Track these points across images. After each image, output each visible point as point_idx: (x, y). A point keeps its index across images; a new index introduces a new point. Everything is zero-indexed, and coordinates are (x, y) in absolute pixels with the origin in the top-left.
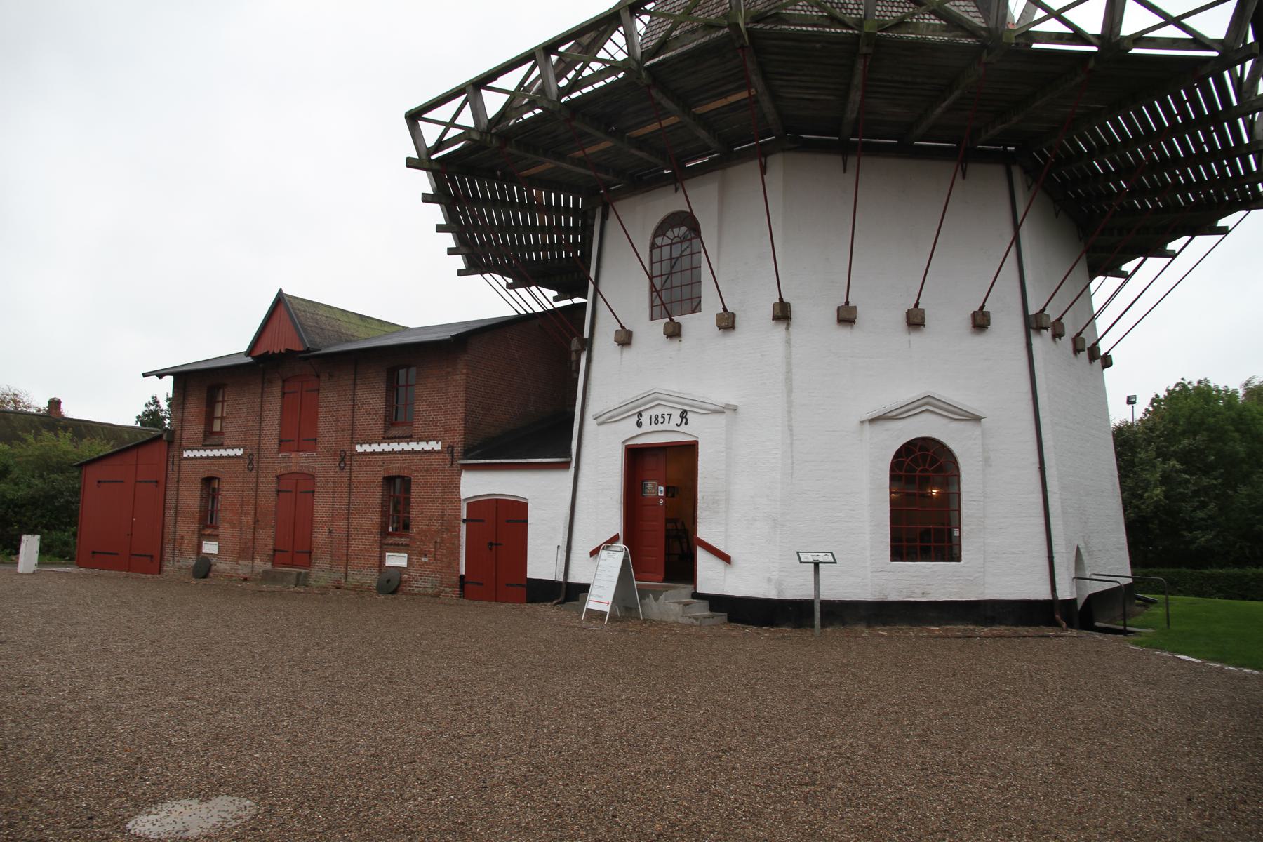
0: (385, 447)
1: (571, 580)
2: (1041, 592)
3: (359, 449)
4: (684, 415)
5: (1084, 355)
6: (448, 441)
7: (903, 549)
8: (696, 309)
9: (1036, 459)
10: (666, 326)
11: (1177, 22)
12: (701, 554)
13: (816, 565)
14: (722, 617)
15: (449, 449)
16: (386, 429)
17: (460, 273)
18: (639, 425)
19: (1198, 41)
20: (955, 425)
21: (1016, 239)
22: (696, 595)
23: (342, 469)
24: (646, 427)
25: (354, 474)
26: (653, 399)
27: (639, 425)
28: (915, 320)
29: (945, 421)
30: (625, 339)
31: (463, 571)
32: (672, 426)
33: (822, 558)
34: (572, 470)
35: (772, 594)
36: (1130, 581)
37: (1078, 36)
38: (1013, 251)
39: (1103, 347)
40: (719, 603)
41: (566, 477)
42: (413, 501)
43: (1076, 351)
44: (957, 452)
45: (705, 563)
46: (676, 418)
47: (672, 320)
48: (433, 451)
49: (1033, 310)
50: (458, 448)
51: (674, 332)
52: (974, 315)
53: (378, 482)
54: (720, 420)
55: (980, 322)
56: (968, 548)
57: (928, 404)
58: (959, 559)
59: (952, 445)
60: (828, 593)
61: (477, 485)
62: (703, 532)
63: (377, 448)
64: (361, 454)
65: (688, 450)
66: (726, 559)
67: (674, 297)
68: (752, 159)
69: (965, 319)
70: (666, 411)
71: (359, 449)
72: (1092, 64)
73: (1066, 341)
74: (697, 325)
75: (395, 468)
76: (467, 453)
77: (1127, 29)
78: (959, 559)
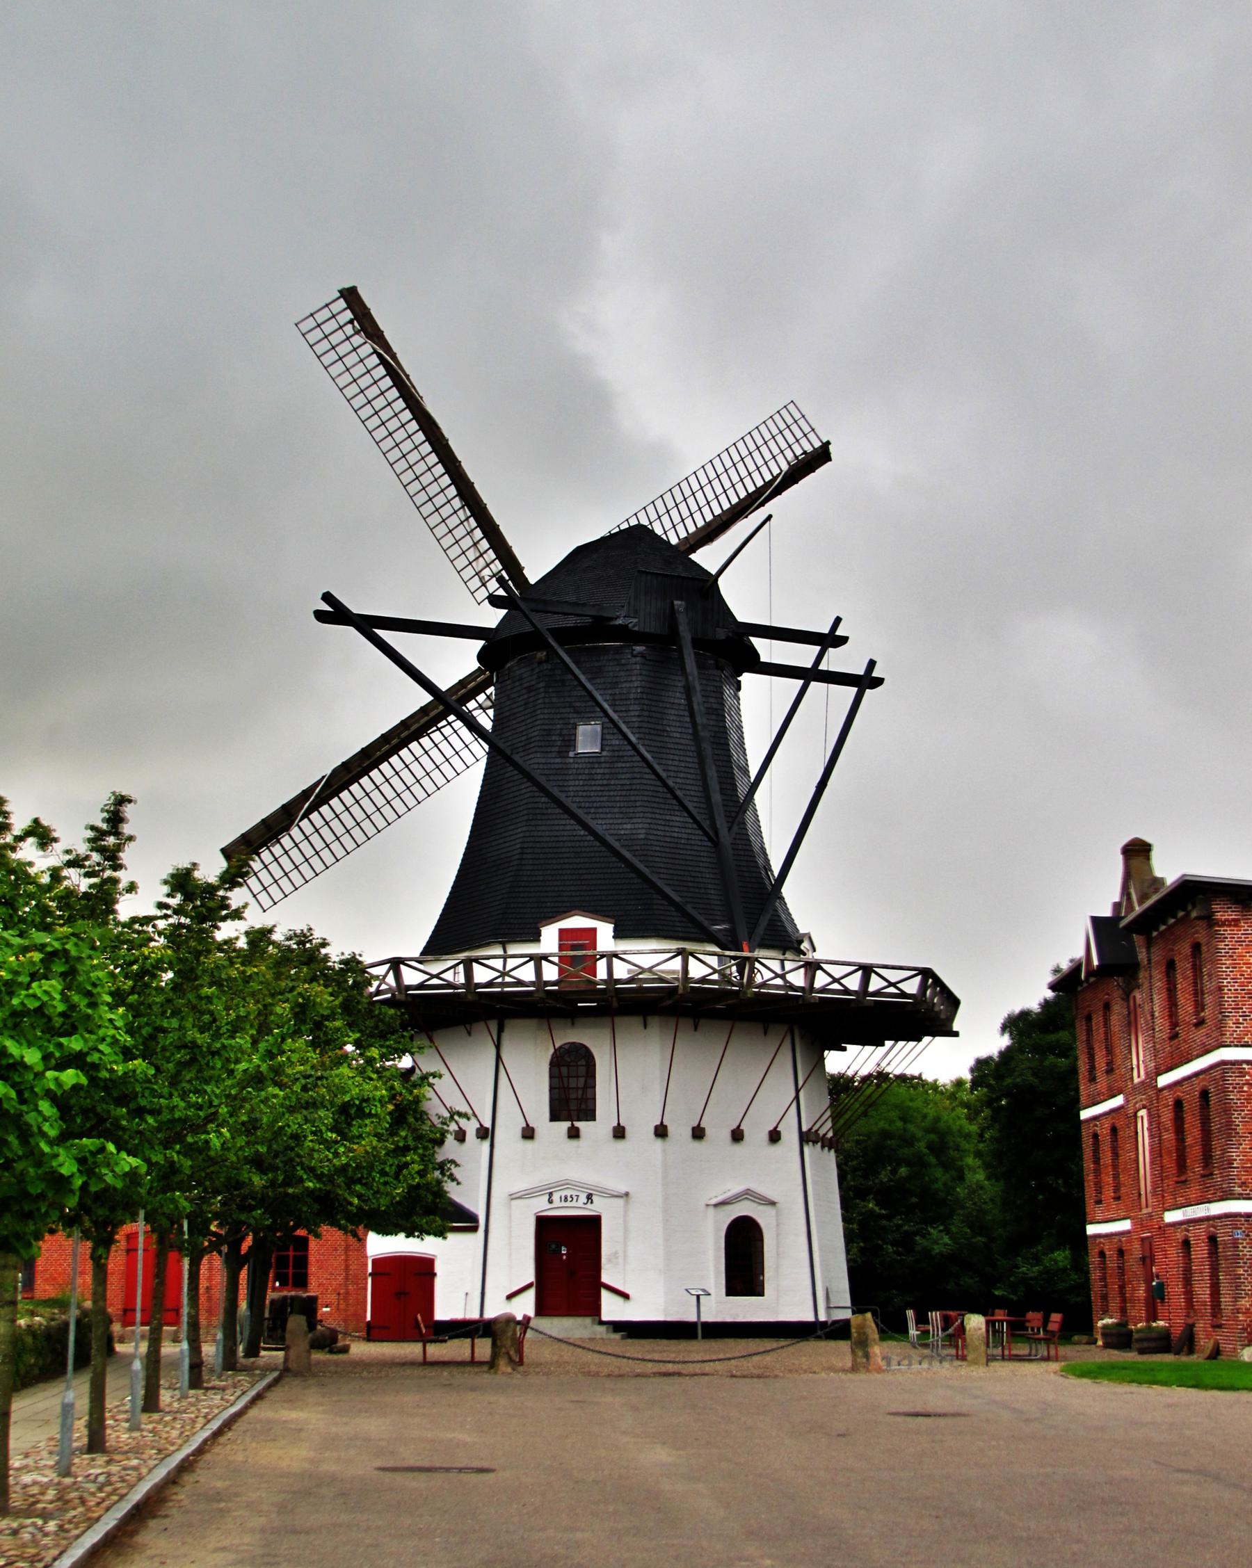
4: (589, 1197)
7: (731, 1291)
8: (590, 1115)
10: (569, 1129)
11: (894, 985)
13: (698, 1297)
14: (617, 1336)
18: (550, 1202)
19: (903, 994)
20: (761, 1207)
21: (797, 1098)
22: (601, 1323)
24: (557, 1203)
26: (566, 1184)
27: (550, 1202)
31: (369, 1318)
32: (580, 1204)
35: (661, 1318)
37: (846, 991)
38: (794, 1104)
40: (617, 1326)
46: (583, 1198)
49: (805, 1129)
51: (574, 1134)
54: (621, 1202)
55: (775, 1136)
57: (748, 1195)
58: (762, 1294)
59: (754, 1216)
60: (707, 1317)
62: (605, 1278)
66: (626, 1296)
67: (572, 1099)
69: (765, 1136)
70: (575, 1193)
72: (853, 1005)
74: (595, 1131)
77: (871, 988)
78: (762, 1294)
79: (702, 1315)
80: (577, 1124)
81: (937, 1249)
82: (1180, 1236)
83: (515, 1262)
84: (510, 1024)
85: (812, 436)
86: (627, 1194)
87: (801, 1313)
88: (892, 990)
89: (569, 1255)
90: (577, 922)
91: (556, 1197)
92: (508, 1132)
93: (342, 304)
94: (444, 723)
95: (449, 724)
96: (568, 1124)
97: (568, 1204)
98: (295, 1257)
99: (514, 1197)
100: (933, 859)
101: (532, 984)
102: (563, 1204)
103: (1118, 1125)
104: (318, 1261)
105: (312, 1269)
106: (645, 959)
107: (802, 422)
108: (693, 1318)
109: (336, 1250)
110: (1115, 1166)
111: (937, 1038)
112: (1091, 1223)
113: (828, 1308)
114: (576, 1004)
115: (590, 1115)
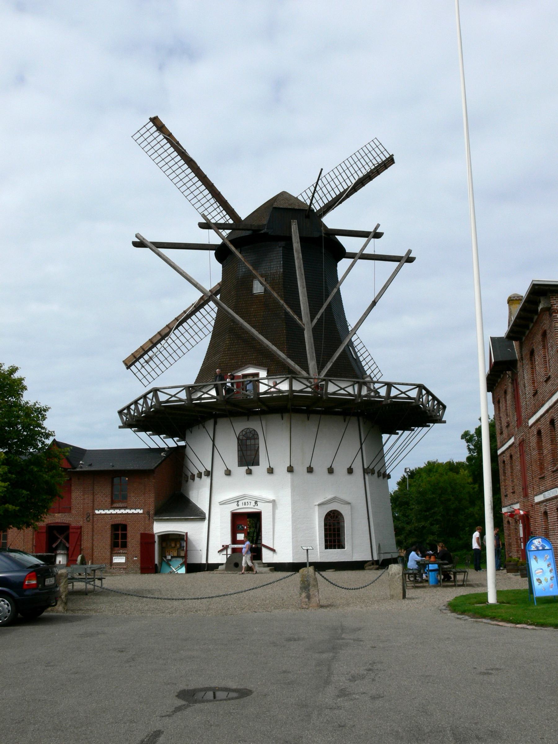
1: (210, 562)
3: (97, 512)
4: (256, 502)
6: (146, 510)
8: (257, 464)
9: (367, 515)
10: (247, 470)
11: (404, 393)
12: (264, 550)
13: (307, 550)
15: (148, 513)
17: (120, 427)
18: (238, 505)
19: (409, 398)
20: (343, 505)
21: (361, 448)
24: (241, 506)
25: (95, 523)
26: (244, 497)
27: (238, 505)
28: (331, 471)
29: (340, 504)
30: (228, 473)
32: (251, 506)
33: (309, 548)
34: (207, 521)
38: (360, 451)
39: (388, 472)
40: (269, 565)
43: (379, 476)
44: (343, 514)
48: (138, 514)
49: (366, 467)
50: (152, 512)
52: (348, 469)
53: (108, 527)
54: (271, 504)
55: (350, 471)
57: (334, 500)
59: (342, 512)
61: (160, 528)
62: (264, 542)
66: (273, 550)
67: (248, 457)
71: (97, 512)
73: (376, 474)
74: (259, 470)
75: (118, 521)
77: (392, 394)
79: (309, 559)
80: (250, 467)
81: (540, 540)
82: (542, 510)
84: (220, 421)
85: (385, 153)
87: (357, 557)
91: (240, 503)
92: (219, 473)
96: (246, 468)
97: (246, 506)
99: (222, 503)
100: (428, 332)
102: (244, 506)
103: (512, 453)
104: (131, 536)
105: (129, 539)
107: (380, 147)
108: (306, 561)
110: (512, 475)
111: (435, 424)
112: (504, 507)
113: (379, 553)
115: (257, 464)
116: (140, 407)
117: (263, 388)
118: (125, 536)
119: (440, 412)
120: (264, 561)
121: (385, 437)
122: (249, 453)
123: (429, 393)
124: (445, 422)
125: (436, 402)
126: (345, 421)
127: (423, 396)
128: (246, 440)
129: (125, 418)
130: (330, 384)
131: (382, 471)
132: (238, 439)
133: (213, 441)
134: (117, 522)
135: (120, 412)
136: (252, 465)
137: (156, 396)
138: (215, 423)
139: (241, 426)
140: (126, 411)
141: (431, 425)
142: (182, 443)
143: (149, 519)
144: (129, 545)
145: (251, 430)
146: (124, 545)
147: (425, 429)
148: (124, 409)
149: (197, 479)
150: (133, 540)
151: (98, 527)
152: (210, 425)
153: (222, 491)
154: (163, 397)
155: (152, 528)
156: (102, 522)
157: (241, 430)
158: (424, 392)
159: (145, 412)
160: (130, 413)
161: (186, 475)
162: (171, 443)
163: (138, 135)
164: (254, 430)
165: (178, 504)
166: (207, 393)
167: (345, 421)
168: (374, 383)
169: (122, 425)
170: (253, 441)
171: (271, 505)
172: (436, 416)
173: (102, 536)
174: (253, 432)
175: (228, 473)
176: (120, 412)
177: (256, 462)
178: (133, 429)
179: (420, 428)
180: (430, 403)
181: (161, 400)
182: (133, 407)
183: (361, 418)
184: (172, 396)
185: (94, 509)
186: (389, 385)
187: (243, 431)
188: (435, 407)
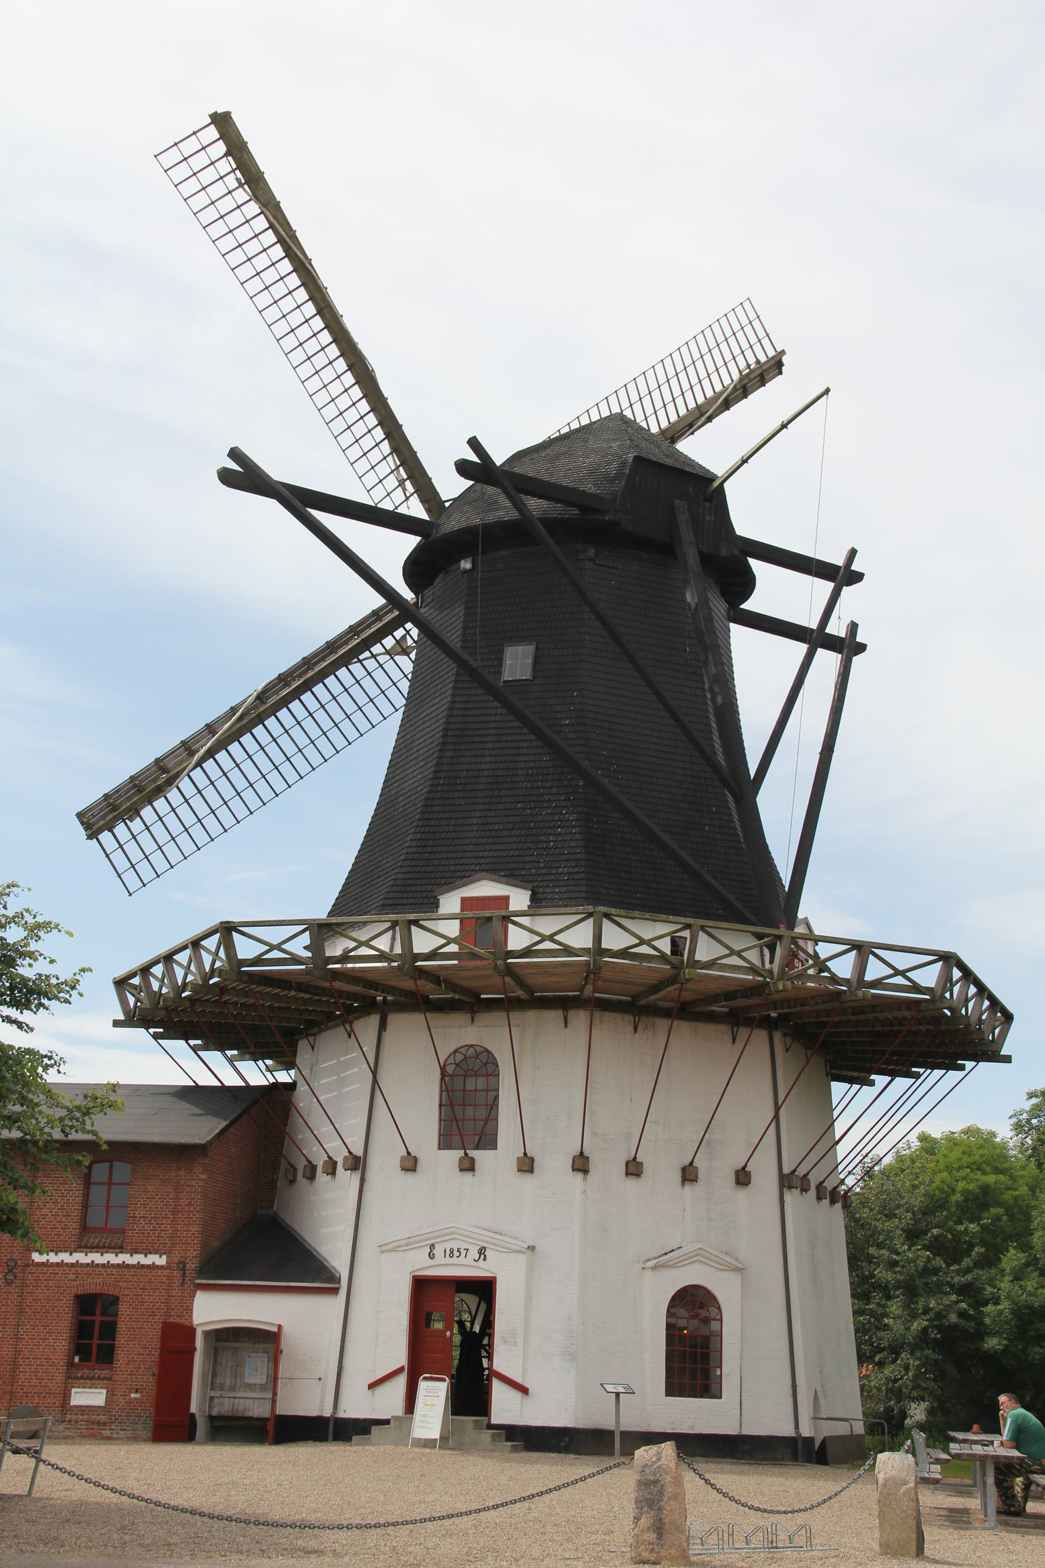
0: (81, 1257)
1: (341, 1415)
2: (784, 1429)
3: (36, 1257)
4: (482, 1251)
5: (826, 1202)
6: (177, 1257)
7: (675, 1386)
10: (461, 1160)
11: (903, 973)
12: (497, 1385)
15: (182, 1266)
16: (80, 1240)
17: (117, 1024)
18: (431, 1256)
19: (916, 988)
20: (720, 1274)
21: (776, 1116)
22: (490, 1426)
23: (8, 1283)
27: (431, 1256)
33: (622, 1390)
36: (655, 429)
41: (334, 1305)
42: (121, 1326)
43: (819, 1198)
45: (499, 1392)
47: (466, 1154)
48: (153, 1267)
49: (786, 1170)
50: (192, 1265)
51: (468, 1166)
55: (743, 1177)
56: (729, 1385)
58: (721, 1398)
61: (213, 1309)
62: (500, 1363)
63: (65, 1257)
64: (38, 1264)
65: (484, 1289)
66: (524, 1390)
67: (468, 1118)
68: (555, 1008)
70: (463, 1246)
71: (36, 1257)
73: (813, 1192)
75: (93, 1285)
76: (203, 1270)
77: (869, 977)
78: (721, 1398)
80: (472, 1153)
83: (383, 1332)
84: (393, 1019)
86: (531, 1248)
88: (899, 980)
89: (454, 1330)
90: (486, 888)
91: (438, 1251)
93: (213, 133)
94: (367, 654)
95: (374, 656)
96: (461, 1153)
98: (101, 1322)
99: (385, 1249)
101: (585, 951)
105: (121, 1340)
106: (545, 933)
109: (153, 1314)
114: (485, 989)
116: (180, 973)
117: (517, 939)
118: (110, 1330)
119: (997, 1031)
120: (494, 1421)
121: (838, 1088)
122: (469, 1112)
123: (968, 975)
124: (1008, 1059)
125: (986, 1003)
126: (734, 1040)
127: (952, 985)
128: (465, 1076)
129: (132, 1000)
130: (702, 937)
131: (829, 1185)
132: (443, 1070)
133: (374, 1073)
134: (93, 1290)
135: (121, 984)
136: (477, 1148)
137: (228, 943)
138: (383, 1026)
139: (460, 1033)
140: (136, 981)
141: (969, 1065)
142: (283, 1077)
143: (183, 1282)
144: (121, 1356)
145: (479, 1049)
146: (107, 1355)
147: (954, 1075)
148: (133, 975)
149: (321, 1178)
150: (136, 1344)
151: (37, 1300)
152: (367, 1027)
153: (391, 1209)
154: (246, 949)
155: (190, 1310)
156: (48, 1288)
157: (453, 1048)
158: (957, 974)
159: (194, 987)
160: (148, 985)
161: (292, 1166)
162: (255, 1074)
163: (174, 156)
164: (488, 1051)
165: (267, 1245)
166: (367, 944)
167: (734, 1040)
168: (817, 940)
169: (121, 1017)
170: (481, 1083)
171: (522, 1260)
172: (982, 1041)
173: (45, 1326)
174: (484, 1057)
175: (410, 1164)
176: (121, 984)
177: (488, 1140)
178: (152, 1031)
179: (938, 1073)
180: (971, 1005)
181: (241, 956)
182: (158, 970)
183: (777, 1036)
184: (272, 947)
185: (29, 1250)
186: (862, 949)
187: (456, 1051)
188: (984, 1017)
